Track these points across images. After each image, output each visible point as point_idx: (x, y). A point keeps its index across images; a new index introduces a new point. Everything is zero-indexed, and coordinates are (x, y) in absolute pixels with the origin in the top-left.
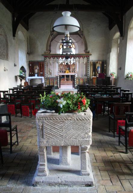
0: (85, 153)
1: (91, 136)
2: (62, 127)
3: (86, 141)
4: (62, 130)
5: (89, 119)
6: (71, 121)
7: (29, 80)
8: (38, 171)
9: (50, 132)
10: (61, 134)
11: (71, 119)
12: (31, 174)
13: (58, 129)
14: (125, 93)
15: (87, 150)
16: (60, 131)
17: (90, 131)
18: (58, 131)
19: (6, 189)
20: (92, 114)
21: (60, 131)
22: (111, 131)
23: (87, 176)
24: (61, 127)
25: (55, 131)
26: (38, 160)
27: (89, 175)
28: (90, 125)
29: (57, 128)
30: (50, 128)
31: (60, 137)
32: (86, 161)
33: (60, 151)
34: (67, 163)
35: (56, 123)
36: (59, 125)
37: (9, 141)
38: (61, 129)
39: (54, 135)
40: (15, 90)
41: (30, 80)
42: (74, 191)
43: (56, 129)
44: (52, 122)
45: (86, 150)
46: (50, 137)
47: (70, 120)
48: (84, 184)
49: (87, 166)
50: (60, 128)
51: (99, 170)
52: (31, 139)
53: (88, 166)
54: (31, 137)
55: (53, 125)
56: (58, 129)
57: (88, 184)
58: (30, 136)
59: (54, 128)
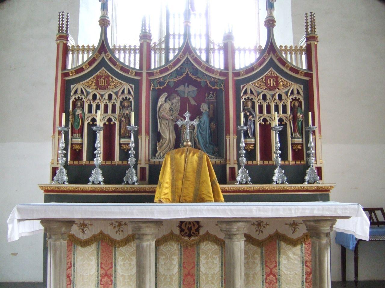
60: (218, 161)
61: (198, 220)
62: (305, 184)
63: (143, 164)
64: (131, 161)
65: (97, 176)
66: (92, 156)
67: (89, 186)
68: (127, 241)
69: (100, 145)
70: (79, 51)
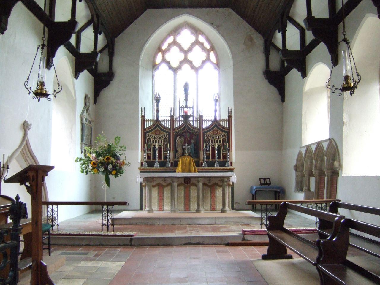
60: (196, 159)
63: (172, 161)
64: (168, 160)
65: (157, 165)
66: (154, 158)
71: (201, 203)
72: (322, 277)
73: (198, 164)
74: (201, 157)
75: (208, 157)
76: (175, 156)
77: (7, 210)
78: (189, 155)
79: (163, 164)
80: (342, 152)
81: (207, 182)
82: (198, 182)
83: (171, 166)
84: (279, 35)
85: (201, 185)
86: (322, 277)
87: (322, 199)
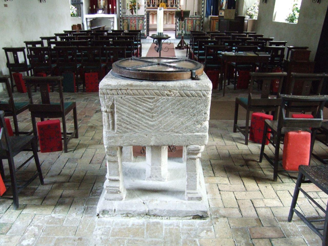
0: (195, 159)
1: (208, 127)
2: (152, 109)
3: (198, 137)
4: (151, 115)
5: (204, 95)
6: (169, 97)
7: (89, 20)
8: (106, 191)
9: (127, 119)
10: (150, 123)
11: (169, 93)
12: (95, 196)
13: (143, 114)
14: (271, 47)
15: (200, 155)
16: (148, 116)
17: (205, 118)
18: (142, 117)
19: (50, 221)
20: (211, 85)
21: (147, 117)
22: (237, 130)
23: (198, 202)
24: (149, 108)
25: (137, 116)
26: (107, 172)
27: (200, 199)
28: (206, 106)
29: (141, 110)
30: (127, 111)
31: (147, 129)
32: (196, 174)
33: (148, 154)
34: (161, 177)
35: (139, 102)
36: (145, 104)
37: (62, 131)
38: (149, 112)
39: (136, 125)
40: (51, 40)
41: (91, 22)
42: (172, 227)
43: (140, 112)
44: (132, 99)
45: (196, 154)
46: (128, 129)
47: (168, 95)
48: (190, 215)
49: (198, 183)
50: (147, 111)
51: (219, 190)
52: (94, 132)
53: (200, 183)
54: (93, 129)
55: (134, 105)
56: (144, 112)
57: (198, 215)
58: (91, 127)
59: (137, 111)
60: (166, 4)
61: (66, 153)
62: (90, 18)
63: (157, 4)
64: (156, 4)
65: (151, 6)
66: (150, 3)
67: (150, 7)
68: (155, 14)
69: (240, 45)
70: (268, 131)
71: (168, 20)
72: (62, 108)
73: (167, 6)
74: (168, 3)
75: (171, 3)
76: (158, 3)
77: (200, 37)
78: (164, 2)
79: (153, 6)
80: (175, 161)
81: (170, 13)
82: (167, 13)
83: (157, 6)
84: (282, 142)
85: (168, 14)
86: (62, 108)
87: (319, 118)
